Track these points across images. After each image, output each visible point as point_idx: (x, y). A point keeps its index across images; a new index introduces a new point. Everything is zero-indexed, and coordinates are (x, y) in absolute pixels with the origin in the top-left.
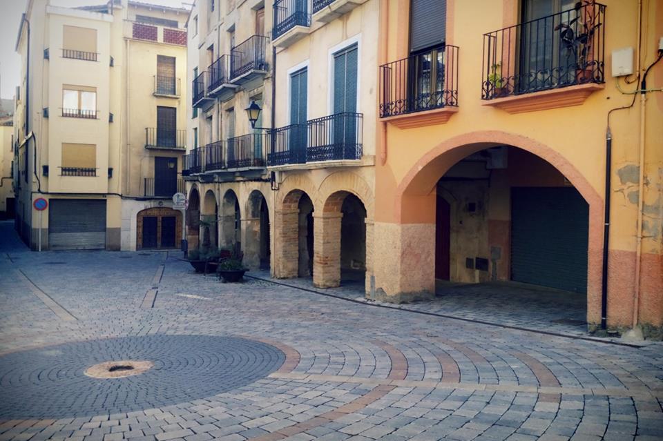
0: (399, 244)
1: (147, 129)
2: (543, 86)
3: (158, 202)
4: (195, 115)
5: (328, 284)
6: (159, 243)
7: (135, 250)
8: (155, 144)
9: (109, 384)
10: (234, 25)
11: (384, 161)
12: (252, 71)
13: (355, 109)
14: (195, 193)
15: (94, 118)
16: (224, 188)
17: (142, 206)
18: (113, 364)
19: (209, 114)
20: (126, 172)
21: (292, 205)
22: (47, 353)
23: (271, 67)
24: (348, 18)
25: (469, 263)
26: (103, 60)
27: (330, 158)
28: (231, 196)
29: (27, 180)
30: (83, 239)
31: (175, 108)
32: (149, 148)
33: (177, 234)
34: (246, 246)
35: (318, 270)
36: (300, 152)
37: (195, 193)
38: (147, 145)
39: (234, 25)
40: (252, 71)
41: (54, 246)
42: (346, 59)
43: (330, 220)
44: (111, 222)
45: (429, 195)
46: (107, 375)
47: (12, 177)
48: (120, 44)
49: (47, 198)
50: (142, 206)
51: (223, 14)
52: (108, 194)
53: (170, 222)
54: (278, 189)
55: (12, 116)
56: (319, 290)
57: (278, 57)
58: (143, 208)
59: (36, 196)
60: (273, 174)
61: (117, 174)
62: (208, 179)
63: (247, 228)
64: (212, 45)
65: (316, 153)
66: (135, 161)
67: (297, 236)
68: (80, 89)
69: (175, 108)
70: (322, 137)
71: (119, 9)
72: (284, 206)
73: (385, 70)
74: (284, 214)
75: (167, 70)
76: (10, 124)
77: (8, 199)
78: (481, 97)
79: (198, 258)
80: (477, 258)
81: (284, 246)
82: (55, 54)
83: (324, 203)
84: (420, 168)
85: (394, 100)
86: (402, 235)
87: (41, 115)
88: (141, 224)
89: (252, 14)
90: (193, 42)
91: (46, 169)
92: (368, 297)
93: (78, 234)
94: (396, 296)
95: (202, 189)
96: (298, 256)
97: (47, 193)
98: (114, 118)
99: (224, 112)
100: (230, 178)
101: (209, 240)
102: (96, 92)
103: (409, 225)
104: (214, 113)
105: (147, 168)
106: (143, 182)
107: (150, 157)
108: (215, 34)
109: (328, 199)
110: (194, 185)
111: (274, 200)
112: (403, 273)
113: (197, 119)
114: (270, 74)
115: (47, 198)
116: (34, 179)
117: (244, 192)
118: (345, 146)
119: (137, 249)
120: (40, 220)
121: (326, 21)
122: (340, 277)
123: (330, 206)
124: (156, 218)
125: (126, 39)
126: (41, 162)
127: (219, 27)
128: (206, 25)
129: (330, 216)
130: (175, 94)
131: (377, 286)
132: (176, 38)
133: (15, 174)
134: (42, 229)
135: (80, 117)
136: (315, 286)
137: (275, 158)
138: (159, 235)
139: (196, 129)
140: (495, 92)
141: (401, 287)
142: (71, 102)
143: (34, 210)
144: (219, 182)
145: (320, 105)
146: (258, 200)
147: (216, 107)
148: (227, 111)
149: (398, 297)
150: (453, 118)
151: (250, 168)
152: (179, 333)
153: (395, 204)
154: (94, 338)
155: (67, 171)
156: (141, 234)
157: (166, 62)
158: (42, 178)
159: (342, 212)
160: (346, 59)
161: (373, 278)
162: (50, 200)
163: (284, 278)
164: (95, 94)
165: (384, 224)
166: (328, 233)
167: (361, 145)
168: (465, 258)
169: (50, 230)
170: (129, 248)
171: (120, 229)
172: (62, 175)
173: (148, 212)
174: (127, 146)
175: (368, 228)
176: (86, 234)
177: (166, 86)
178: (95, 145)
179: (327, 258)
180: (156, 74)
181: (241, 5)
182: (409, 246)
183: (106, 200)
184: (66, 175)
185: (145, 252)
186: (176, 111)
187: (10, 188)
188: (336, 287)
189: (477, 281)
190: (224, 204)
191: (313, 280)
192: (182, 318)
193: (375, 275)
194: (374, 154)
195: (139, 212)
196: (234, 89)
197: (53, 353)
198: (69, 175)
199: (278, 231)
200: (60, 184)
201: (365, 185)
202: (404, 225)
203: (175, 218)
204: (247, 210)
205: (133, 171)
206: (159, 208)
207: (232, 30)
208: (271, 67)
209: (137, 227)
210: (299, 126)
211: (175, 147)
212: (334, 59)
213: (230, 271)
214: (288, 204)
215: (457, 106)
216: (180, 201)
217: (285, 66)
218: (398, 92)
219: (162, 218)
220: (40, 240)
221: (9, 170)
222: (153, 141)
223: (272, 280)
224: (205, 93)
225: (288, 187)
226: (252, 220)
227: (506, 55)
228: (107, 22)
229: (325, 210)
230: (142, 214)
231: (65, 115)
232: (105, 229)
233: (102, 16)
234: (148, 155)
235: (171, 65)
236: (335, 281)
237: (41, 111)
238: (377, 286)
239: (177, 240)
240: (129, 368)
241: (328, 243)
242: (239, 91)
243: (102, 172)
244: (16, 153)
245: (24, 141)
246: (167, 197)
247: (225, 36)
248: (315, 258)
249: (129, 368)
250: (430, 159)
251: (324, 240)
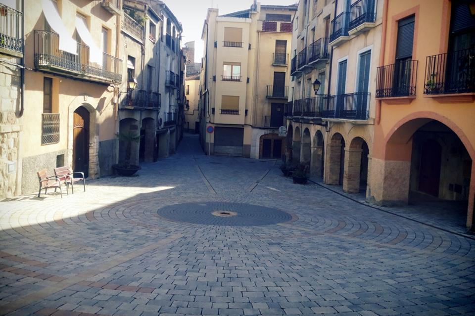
0: (383, 172)
1: (267, 86)
3: (272, 130)
4: (293, 80)
5: (351, 191)
6: (272, 155)
7: (258, 158)
8: (272, 95)
9: (230, 224)
10: (315, 27)
11: (379, 122)
12: (319, 59)
13: (367, 91)
14: (291, 126)
15: (239, 80)
16: (304, 126)
17: (263, 132)
18: (223, 212)
19: (299, 80)
20: (255, 112)
21: (337, 141)
22: (201, 204)
23: (330, 57)
24: (368, 34)
25: (451, 187)
26: (245, 46)
28: (307, 131)
29: (204, 116)
30: (230, 150)
31: (285, 73)
32: (268, 98)
34: (313, 163)
35: (345, 182)
36: (342, 113)
37: (291, 126)
38: (267, 96)
39: (315, 27)
40: (319, 59)
41: (216, 153)
42: (365, 56)
43: (354, 153)
44: (246, 141)
45: (407, 143)
46: (219, 215)
47: (198, 110)
48: (255, 34)
49: (213, 126)
50: (263, 132)
51: (310, 19)
52: (245, 125)
53: (279, 142)
54: (329, 131)
55: (200, 73)
56: (345, 194)
57: (334, 51)
58: (263, 134)
59: (208, 125)
60: (327, 122)
61: (250, 114)
62: (297, 121)
63: (314, 152)
64: (304, 38)
65: (349, 114)
66: (260, 106)
67: (339, 160)
68: (232, 64)
69: (285, 73)
70: (350, 105)
71: (256, 14)
72: (332, 142)
73: (382, 69)
74: (332, 146)
75: (282, 49)
76: (198, 79)
77: (196, 122)
78: (423, 93)
79: (285, 168)
80: (456, 185)
81: (331, 166)
82: (220, 44)
83: (350, 142)
84: (396, 129)
86: (386, 167)
87: (212, 80)
88: (262, 143)
89: (324, 21)
90: (296, 33)
91: (213, 110)
92: (367, 201)
93: (228, 147)
94: (380, 201)
95: (295, 125)
96: (339, 172)
97: (213, 123)
98: (250, 80)
99: (306, 80)
100: (307, 122)
101: (292, 158)
102: (240, 66)
103: (391, 161)
104: (301, 80)
105: (267, 109)
107: (269, 103)
108: (305, 31)
109: (352, 141)
110: (290, 123)
111: (327, 137)
112: (385, 189)
113: (294, 82)
114: (329, 61)
115: (213, 126)
116: (208, 115)
117: (313, 130)
118: (361, 113)
119: (259, 158)
120: (210, 138)
121: (358, 34)
122: (359, 187)
123: (354, 145)
124: (270, 140)
125: (258, 32)
126: (211, 106)
127: (307, 27)
128: (302, 24)
129: (354, 151)
130: (285, 64)
131: (371, 195)
132: (287, 28)
133: (200, 109)
134: (211, 143)
135: (231, 81)
136: (344, 191)
137: (328, 114)
139: (293, 88)
140: (433, 90)
141: (383, 196)
142: (227, 71)
143: (207, 132)
144: (302, 123)
145: (351, 87)
146: (319, 134)
147: (303, 76)
148: (308, 79)
149: (381, 203)
150: (413, 102)
151: (315, 118)
152: (255, 204)
153: (383, 150)
154: (220, 201)
155: (225, 111)
157: (281, 44)
158: (211, 115)
159: (362, 148)
160: (365, 56)
161: (370, 189)
162: (215, 127)
163: (330, 184)
164: (239, 67)
165: (376, 159)
166: (352, 161)
167: (369, 111)
169: (215, 144)
171: (250, 145)
172: (221, 113)
173: (266, 136)
174: (256, 96)
175: (369, 160)
176: (233, 147)
177: (279, 58)
178: (239, 97)
179: (351, 175)
180: (274, 52)
181: (319, 15)
182: (390, 173)
183: (243, 128)
184: (223, 114)
185: (263, 160)
186: (285, 75)
187: (197, 116)
188: (356, 193)
189: (454, 199)
190: (304, 136)
192: (260, 198)
193: (371, 188)
194: (374, 118)
195: (262, 136)
196: (312, 67)
197: (203, 205)
198: (225, 114)
199: (328, 156)
200: (220, 119)
201: (370, 135)
202: (387, 161)
204: (314, 141)
205: (259, 112)
207: (314, 30)
208: (330, 57)
209: (260, 145)
210: (342, 96)
211: (283, 97)
212: (360, 57)
213: (297, 177)
214: (334, 141)
215: (415, 95)
216: (282, 131)
217: (337, 58)
218: (388, 84)
219: (274, 140)
220: (210, 149)
221: (197, 106)
222: (271, 93)
223: (322, 185)
224: (297, 68)
225: (334, 131)
226: (317, 148)
227: (440, 69)
228: (248, 23)
229: (351, 147)
231: (224, 80)
232: (242, 145)
233: (246, 20)
234: (267, 102)
235: (284, 46)
236: (356, 190)
237: (212, 77)
238: (371, 195)
240: (228, 214)
241: (352, 166)
242: (314, 69)
243: (242, 112)
244: (201, 97)
245: (204, 93)
247: (310, 33)
248: (345, 175)
249: (228, 214)
250: (401, 124)
251: (349, 164)
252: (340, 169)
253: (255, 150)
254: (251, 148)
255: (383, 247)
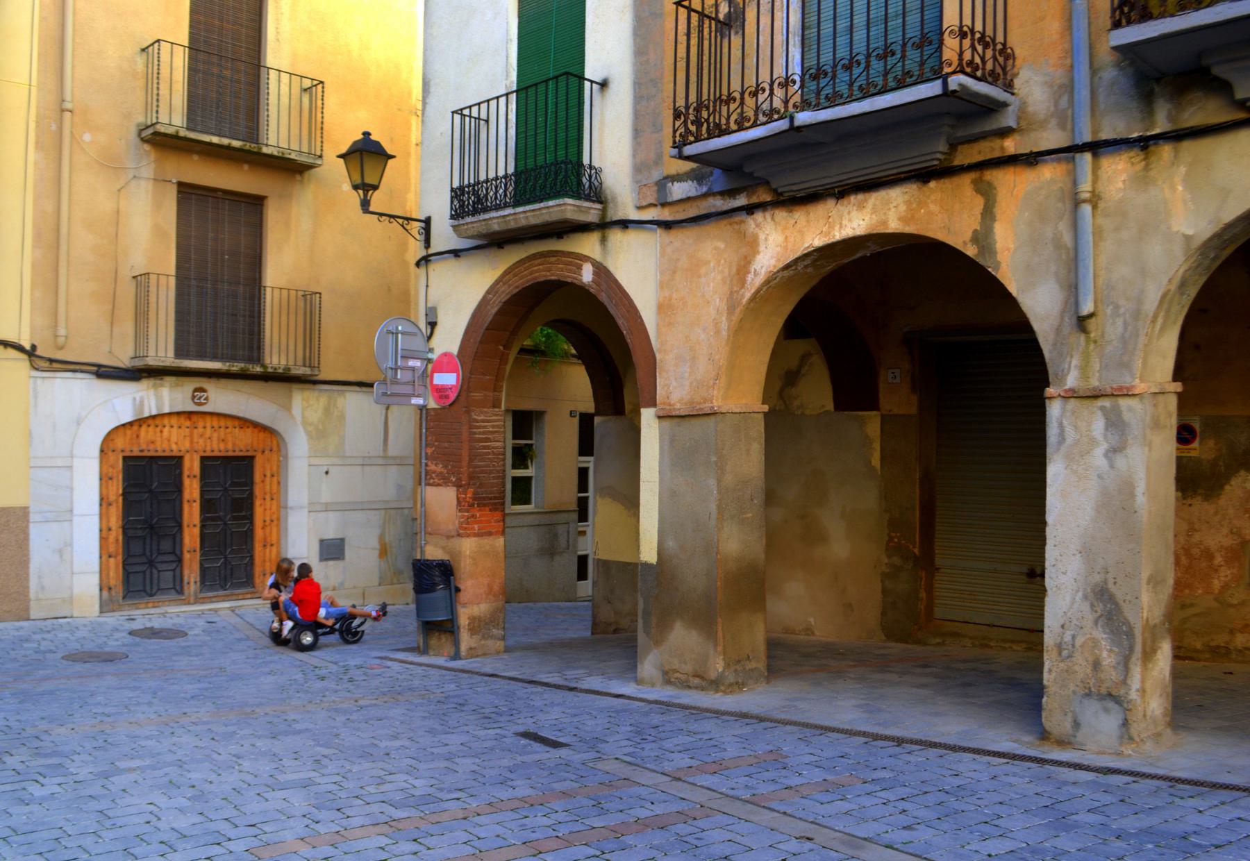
2: (757, 119)
3: (190, 385)
6: (191, 574)
27: (32, 321)
33: (259, 533)
85: (736, 86)
88: (116, 488)
106: (127, 292)
107: (159, 180)
138: (191, 536)
156: (116, 534)
168: (383, 601)
170: (70, 600)
171: (24, 512)
173: (146, 434)
191: (636, 672)
203: (252, 458)
206: (189, 414)
230: (120, 442)
234: (148, 171)
239: (264, 560)
246: (236, 367)
252: (598, 692)
253: (64, 550)
254: (34, 531)
255: (151, 584)
